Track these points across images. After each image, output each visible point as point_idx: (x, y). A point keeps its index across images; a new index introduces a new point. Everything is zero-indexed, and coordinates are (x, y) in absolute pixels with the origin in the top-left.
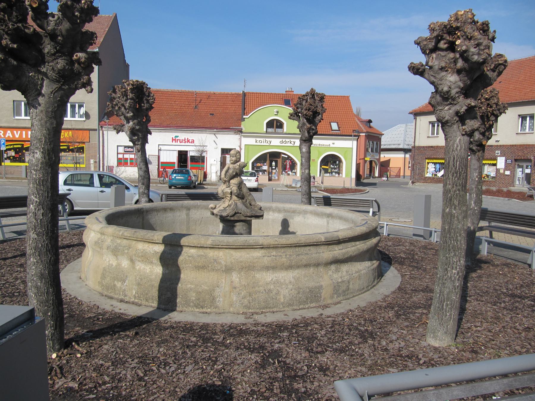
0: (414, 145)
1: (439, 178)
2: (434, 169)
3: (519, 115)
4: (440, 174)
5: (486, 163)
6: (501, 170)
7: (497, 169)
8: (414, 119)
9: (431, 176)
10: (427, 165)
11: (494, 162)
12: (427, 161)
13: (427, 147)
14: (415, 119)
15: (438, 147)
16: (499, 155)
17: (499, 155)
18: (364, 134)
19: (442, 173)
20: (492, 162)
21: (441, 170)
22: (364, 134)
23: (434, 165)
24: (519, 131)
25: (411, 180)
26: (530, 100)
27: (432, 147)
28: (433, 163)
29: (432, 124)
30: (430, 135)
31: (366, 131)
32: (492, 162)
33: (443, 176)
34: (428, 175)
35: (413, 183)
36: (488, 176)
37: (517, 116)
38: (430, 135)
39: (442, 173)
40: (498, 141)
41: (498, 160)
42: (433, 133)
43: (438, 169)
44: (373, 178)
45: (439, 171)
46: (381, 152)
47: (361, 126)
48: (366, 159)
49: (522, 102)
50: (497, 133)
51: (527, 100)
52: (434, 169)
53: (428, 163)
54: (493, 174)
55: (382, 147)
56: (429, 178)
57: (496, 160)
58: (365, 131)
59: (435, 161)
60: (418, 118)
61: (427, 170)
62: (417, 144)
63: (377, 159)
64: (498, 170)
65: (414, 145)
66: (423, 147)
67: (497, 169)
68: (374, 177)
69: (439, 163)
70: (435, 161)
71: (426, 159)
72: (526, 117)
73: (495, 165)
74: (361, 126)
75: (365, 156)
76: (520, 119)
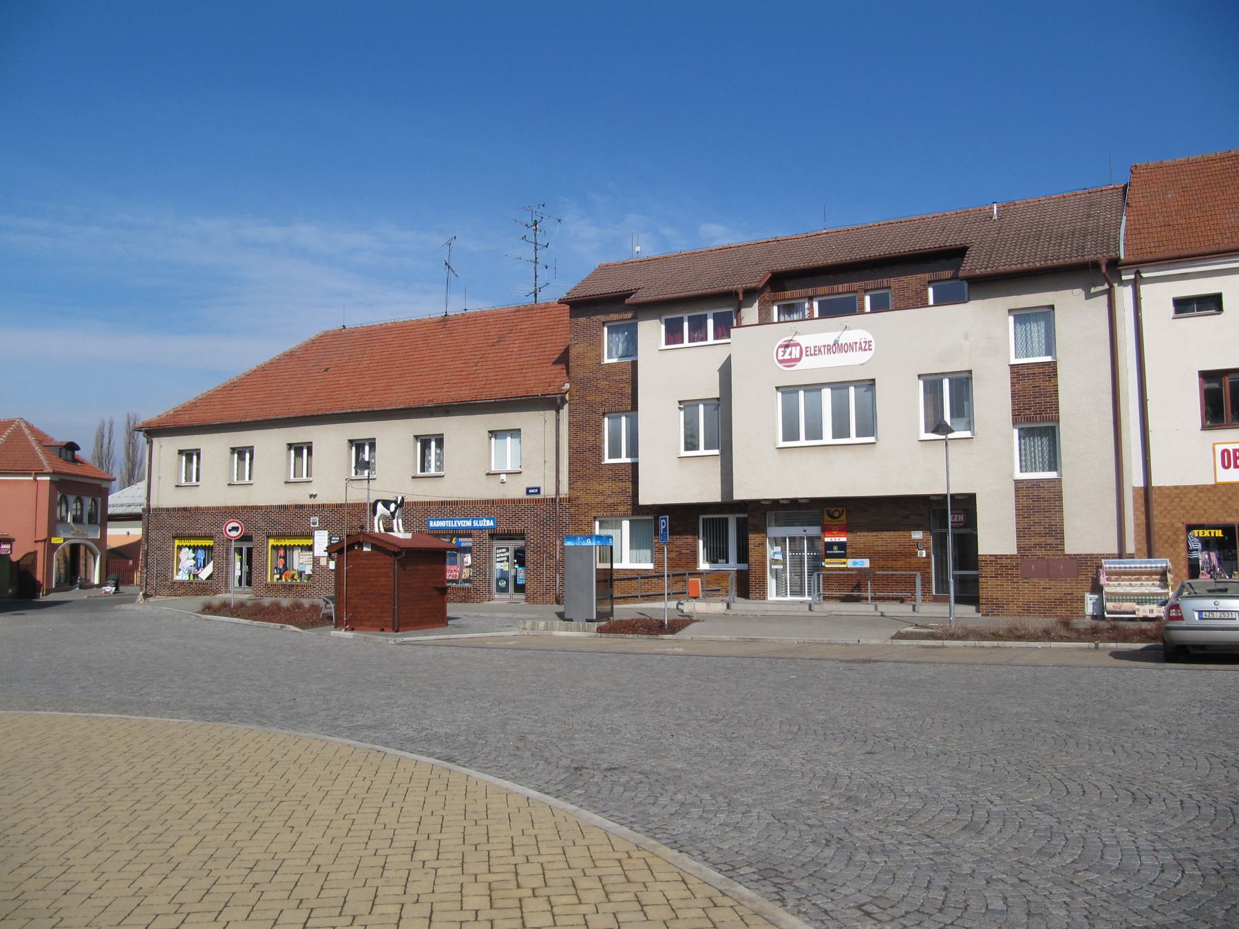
0: (148, 505)
1: (202, 583)
2: (193, 562)
3: (351, 441)
4: (204, 574)
5: (294, 545)
6: (321, 559)
7: (314, 558)
8: (148, 442)
9: (186, 577)
10: (178, 553)
11: (309, 542)
12: (177, 543)
13: (174, 509)
14: (150, 443)
15: (197, 509)
16: (317, 525)
17: (317, 525)
18: (48, 478)
19: (209, 569)
20: (724, 521)
21: (208, 563)
22: (48, 478)
23: (194, 552)
24: (235, 480)
25: (141, 590)
26: (365, 410)
27: (185, 509)
28: (190, 547)
29: (296, 449)
30: (419, 473)
31: (51, 471)
32: (724, 521)
33: (210, 577)
34: (182, 576)
35: (146, 596)
36: (301, 574)
37: (346, 443)
38: (419, 473)
39: (209, 569)
40: (315, 496)
41: (316, 538)
42: (240, 475)
43: (201, 561)
44: (81, 587)
45: (204, 567)
46: (109, 523)
47: (42, 457)
48: (55, 540)
49: (352, 413)
50: (443, 473)
51: (359, 410)
52: (193, 562)
53: (180, 548)
54: (308, 570)
55: (110, 511)
56: (182, 583)
57: (311, 536)
58: (49, 470)
59: (193, 543)
60: (155, 440)
61: (178, 565)
62: (154, 504)
63: (94, 541)
64: (316, 560)
65: (148, 505)
66: (168, 509)
67: (314, 558)
68: (86, 585)
69: (204, 548)
70: (193, 543)
71: (174, 538)
72: (430, 441)
73: (310, 548)
74: (42, 457)
75: (52, 532)
76: (354, 448)
